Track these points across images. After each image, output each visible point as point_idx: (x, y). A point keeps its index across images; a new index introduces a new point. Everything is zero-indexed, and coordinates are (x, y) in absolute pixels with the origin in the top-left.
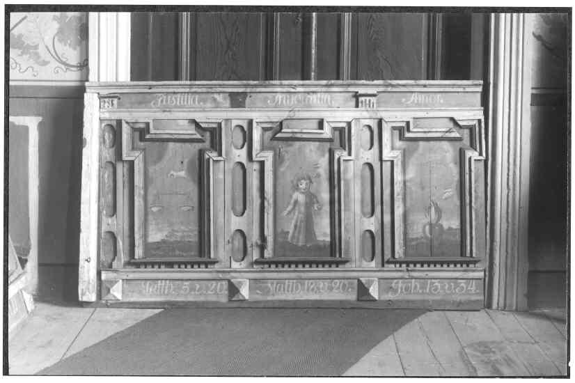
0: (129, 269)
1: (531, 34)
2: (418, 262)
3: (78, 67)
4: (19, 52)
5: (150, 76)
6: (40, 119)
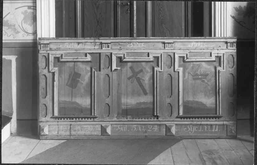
0: (52, 120)
2: (69, 118)
3: (32, 34)
4: (7, 28)
6: (17, 56)
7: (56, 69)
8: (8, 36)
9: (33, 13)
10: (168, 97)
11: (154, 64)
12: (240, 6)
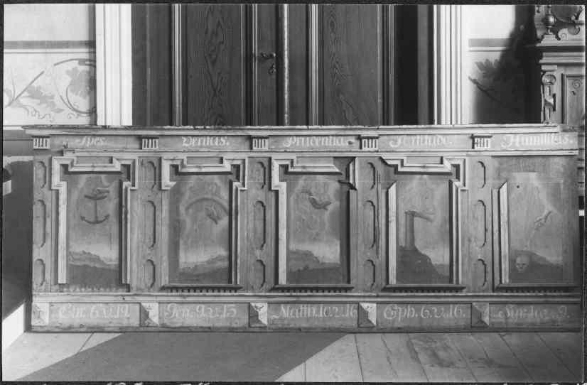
1: (467, 78)
3: (86, 113)
7: (284, 185)
8: (41, 117)
9: (89, 73)
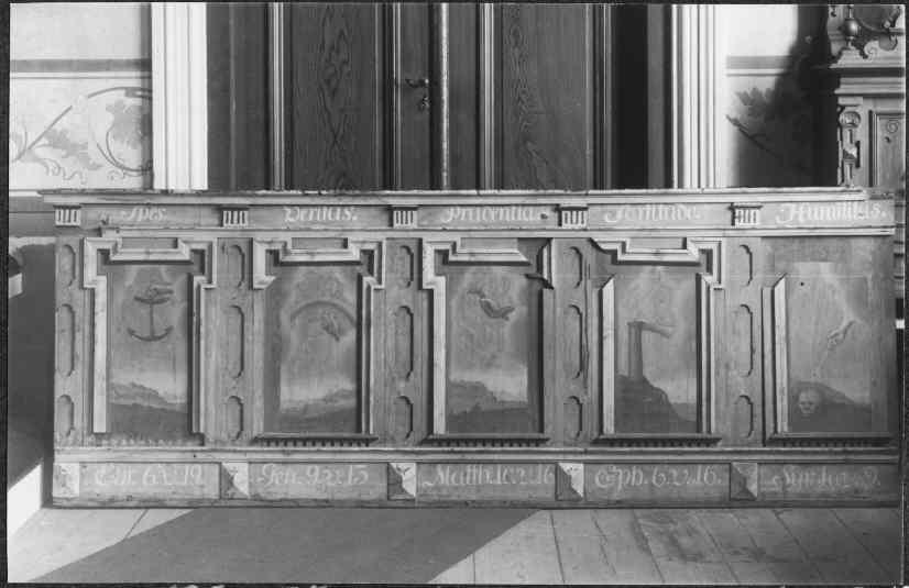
1: (724, 117)
3: (137, 171)
5: (609, 185)
9: (141, 108)
10: (400, 378)
11: (361, 269)
12: (738, 94)
